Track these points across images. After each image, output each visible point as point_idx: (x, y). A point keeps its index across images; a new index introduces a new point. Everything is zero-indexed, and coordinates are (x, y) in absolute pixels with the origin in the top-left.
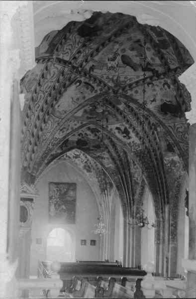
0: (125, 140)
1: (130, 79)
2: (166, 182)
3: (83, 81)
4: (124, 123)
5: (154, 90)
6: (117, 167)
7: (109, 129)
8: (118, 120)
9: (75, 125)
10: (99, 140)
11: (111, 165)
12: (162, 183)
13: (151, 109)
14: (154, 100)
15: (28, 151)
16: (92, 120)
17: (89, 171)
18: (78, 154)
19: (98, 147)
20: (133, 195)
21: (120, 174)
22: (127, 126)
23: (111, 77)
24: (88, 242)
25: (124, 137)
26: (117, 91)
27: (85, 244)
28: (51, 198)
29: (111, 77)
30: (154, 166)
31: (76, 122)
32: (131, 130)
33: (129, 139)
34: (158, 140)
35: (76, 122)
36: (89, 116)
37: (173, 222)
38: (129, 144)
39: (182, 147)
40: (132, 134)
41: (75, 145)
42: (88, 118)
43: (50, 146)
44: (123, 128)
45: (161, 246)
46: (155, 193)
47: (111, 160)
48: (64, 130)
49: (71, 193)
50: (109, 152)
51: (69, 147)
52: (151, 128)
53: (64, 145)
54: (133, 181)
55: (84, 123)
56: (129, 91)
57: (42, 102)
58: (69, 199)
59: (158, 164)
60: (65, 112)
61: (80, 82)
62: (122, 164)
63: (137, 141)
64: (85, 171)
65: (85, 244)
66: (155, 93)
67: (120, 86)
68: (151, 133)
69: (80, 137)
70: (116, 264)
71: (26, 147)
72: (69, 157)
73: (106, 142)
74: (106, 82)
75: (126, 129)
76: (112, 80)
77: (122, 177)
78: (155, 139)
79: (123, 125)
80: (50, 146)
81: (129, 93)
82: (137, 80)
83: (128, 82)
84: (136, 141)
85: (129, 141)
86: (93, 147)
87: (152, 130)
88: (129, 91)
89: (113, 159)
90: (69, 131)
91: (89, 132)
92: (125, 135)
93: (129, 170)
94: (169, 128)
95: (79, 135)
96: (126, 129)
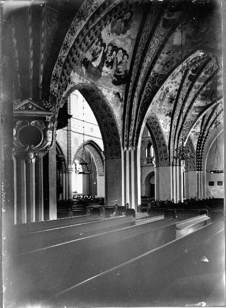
9: (181, 56)
31: (180, 53)
36: (196, 41)
90: (173, 65)
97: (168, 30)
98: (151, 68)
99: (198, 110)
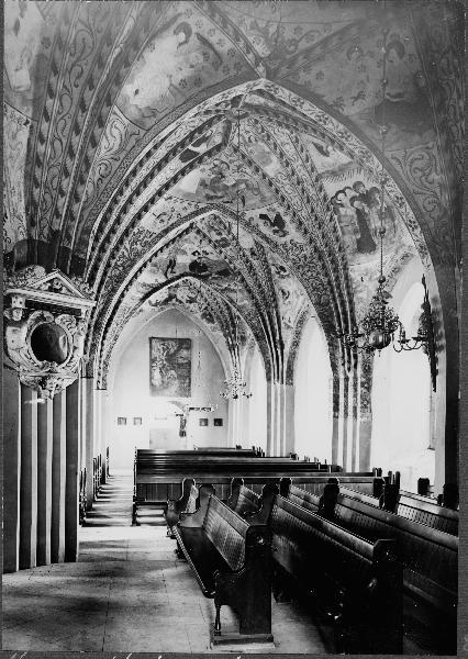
0: (275, 238)
1: (308, 36)
2: (352, 311)
3: (194, 30)
4: (275, 206)
5: (364, 68)
6: (256, 305)
7: (247, 219)
8: (263, 200)
10: (227, 260)
11: (246, 302)
12: (345, 313)
13: (353, 119)
14: (360, 96)
15: (62, 194)
16: (215, 201)
17: (211, 320)
18: (193, 296)
19: (225, 273)
20: (282, 348)
21: (261, 315)
22: (281, 210)
23: (262, 25)
24: (211, 422)
25: (275, 232)
26: (277, 71)
27: (206, 425)
28: (153, 361)
29: (262, 25)
30: (329, 283)
32: (287, 219)
33: (284, 236)
34: (340, 233)
35: (185, 204)
36: (212, 194)
37: (364, 380)
38: (284, 245)
39: (420, 204)
40: (291, 227)
41: (188, 270)
42: (209, 197)
43: (139, 247)
44: (272, 216)
45: (341, 420)
46: (329, 328)
47: (246, 293)
48: (163, 217)
49: (184, 353)
50: (243, 280)
51: (177, 274)
52: (328, 209)
53: (170, 270)
54: (283, 325)
55: (201, 206)
56: (302, 74)
57: (90, 59)
58: (181, 361)
59: (337, 278)
60: (154, 116)
61: (186, 29)
62: (264, 298)
63: (299, 238)
64: (204, 321)
65: (206, 425)
66: (363, 76)
67: (165, 513)
68: (328, 218)
69: (196, 258)
70: (290, 460)
71: (55, 184)
72: (181, 302)
73: (239, 264)
74: (251, 39)
75: (278, 216)
76: (265, 32)
77: (264, 320)
78: (335, 230)
79: (274, 210)
80: (139, 247)
81: (303, 77)
82: (308, 45)
83: (303, 45)
84: (296, 240)
85: (283, 240)
86: (219, 273)
87: (329, 213)
88: (302, 74)
89: (250, 291)
91: (209, 249)
92: (276, 228)
93: (276, 306)
94: (394, 162)
95: (194, 254)
96: (278, 216)
97: (184, 165)
98: (139, 216)
99: (141, 289)
